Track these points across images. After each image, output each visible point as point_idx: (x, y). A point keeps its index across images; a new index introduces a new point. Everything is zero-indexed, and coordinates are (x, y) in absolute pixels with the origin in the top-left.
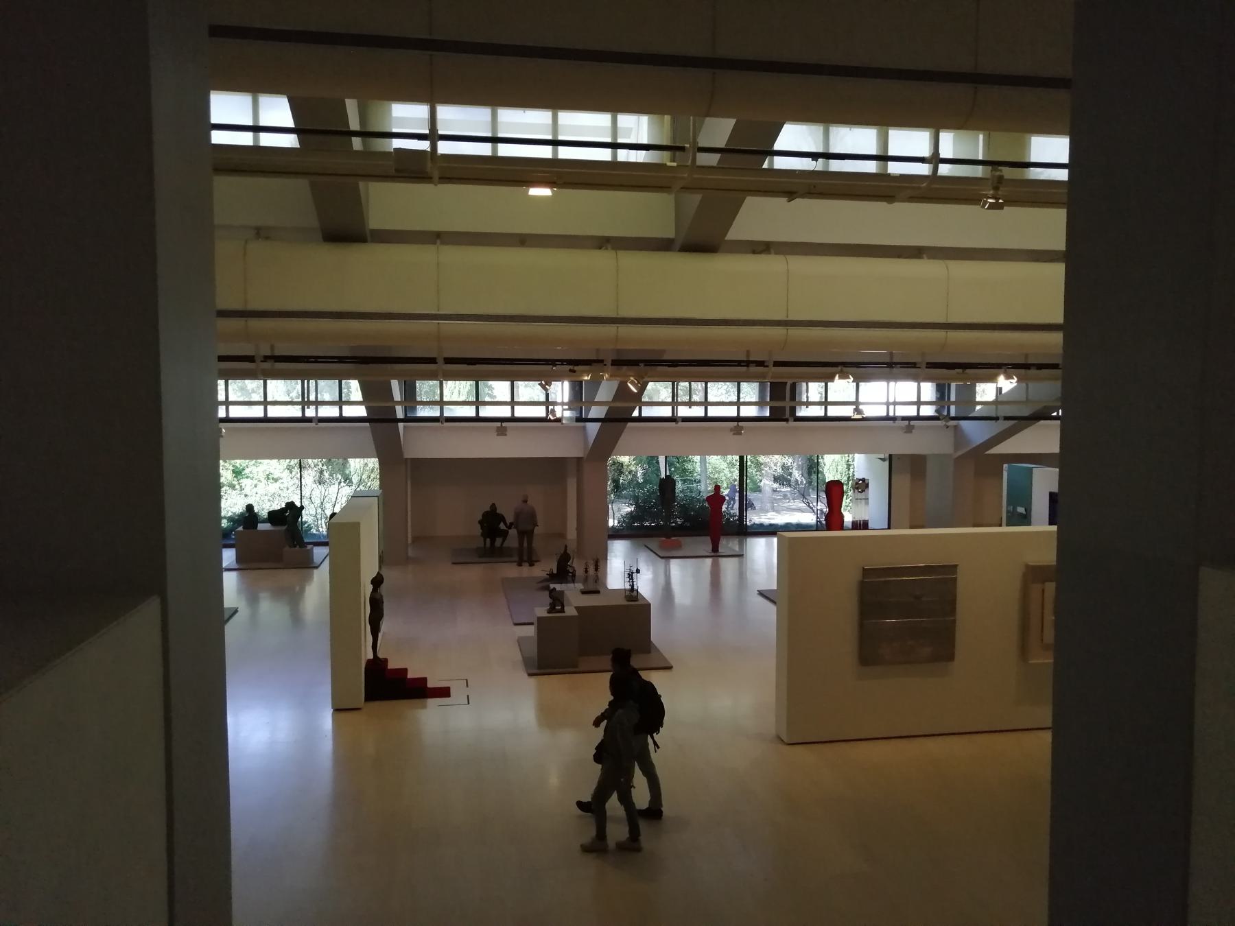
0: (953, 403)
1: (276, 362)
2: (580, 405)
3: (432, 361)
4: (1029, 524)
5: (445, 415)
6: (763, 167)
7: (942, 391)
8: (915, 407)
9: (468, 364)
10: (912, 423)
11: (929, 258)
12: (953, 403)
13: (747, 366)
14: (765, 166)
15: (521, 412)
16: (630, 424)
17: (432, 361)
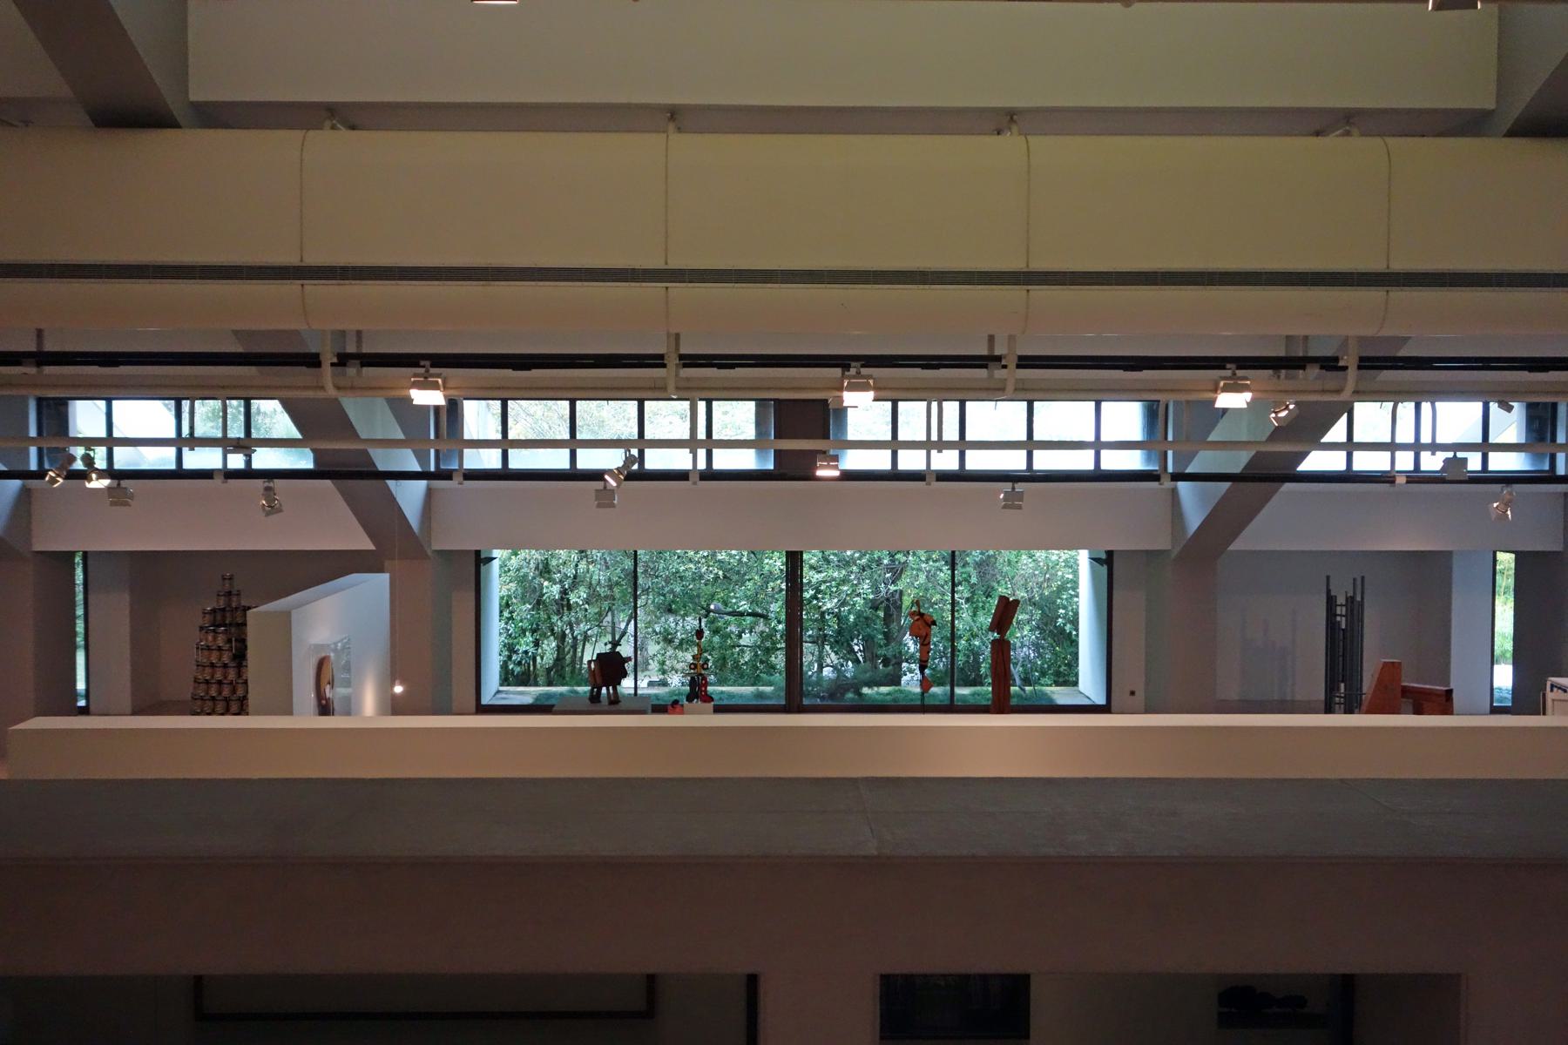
0: (1562, 447)
1: (363, 365)
2: (1548, 450)
3: (657, 361)
4: (242, 711)
5: (465, 467)
10: (1020, 487)
11: (1363, 135)
12: (1562, 447)
13: (39, 364)
15: (1046, 461)
16: (1288, 486)
17: (657, 361)
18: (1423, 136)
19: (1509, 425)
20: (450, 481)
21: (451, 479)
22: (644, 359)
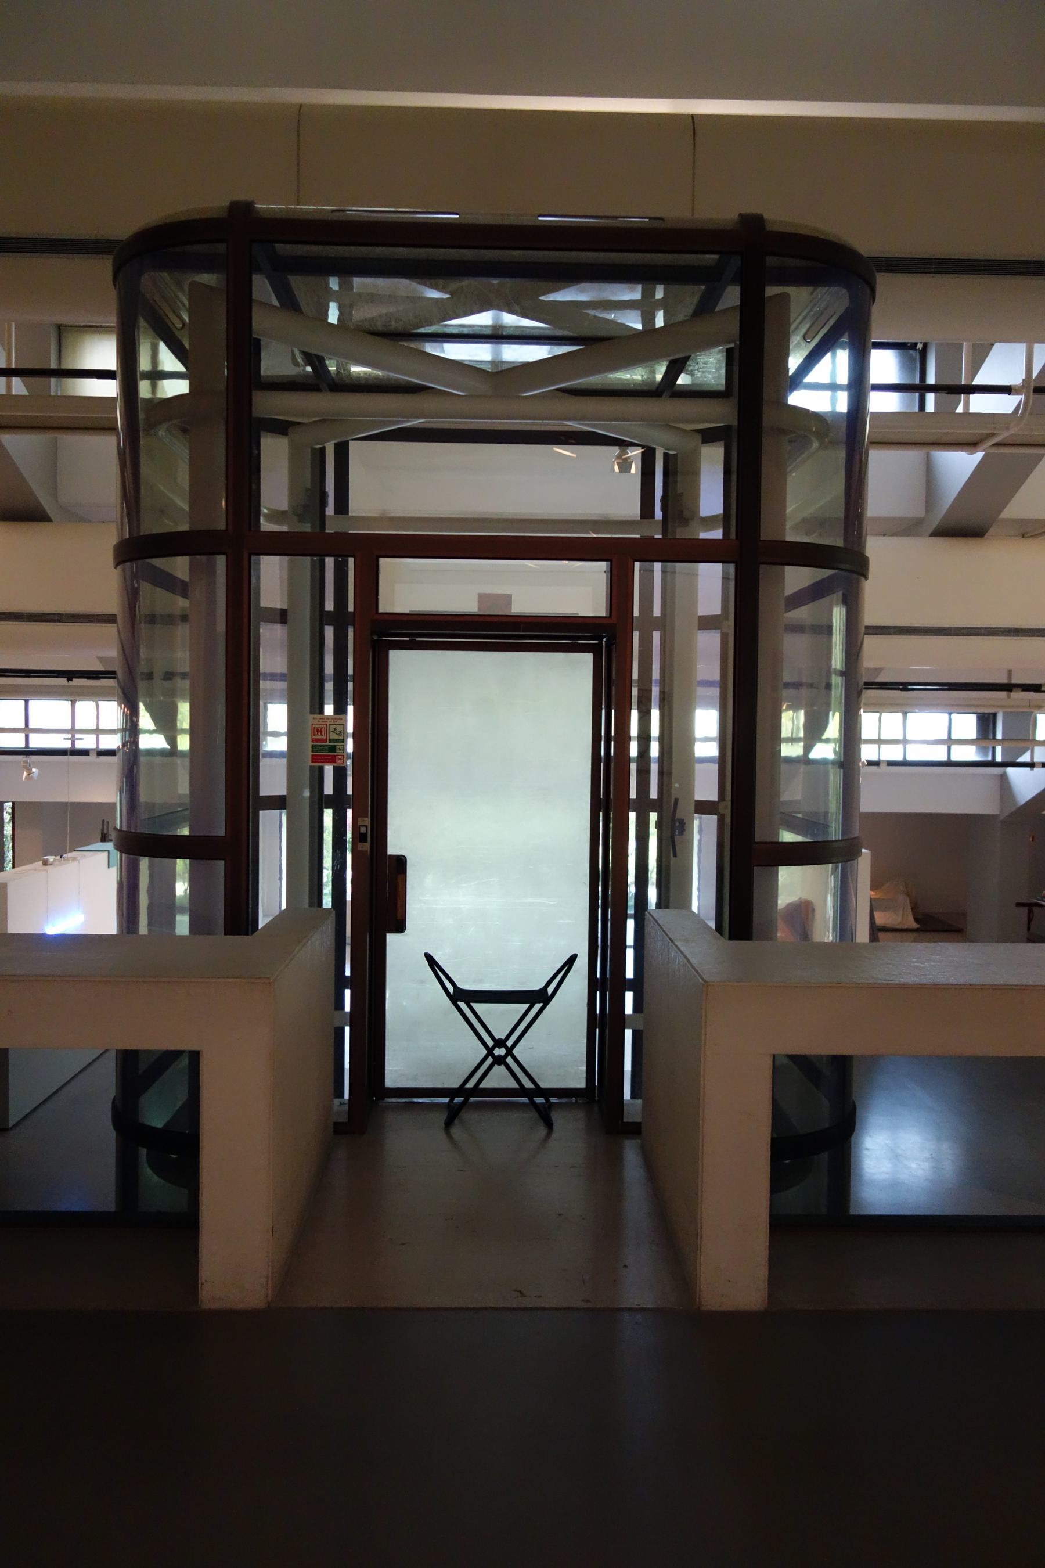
2: (990, 745)
6: (957, 411)
7: (986, 724)
8: (945, 747)
9: (89, 678)
14: (960, 410)
18: (884, 535)
19: (967, 725)
20: (88, 757)
21: (89, 755)
22: (99, 674)
